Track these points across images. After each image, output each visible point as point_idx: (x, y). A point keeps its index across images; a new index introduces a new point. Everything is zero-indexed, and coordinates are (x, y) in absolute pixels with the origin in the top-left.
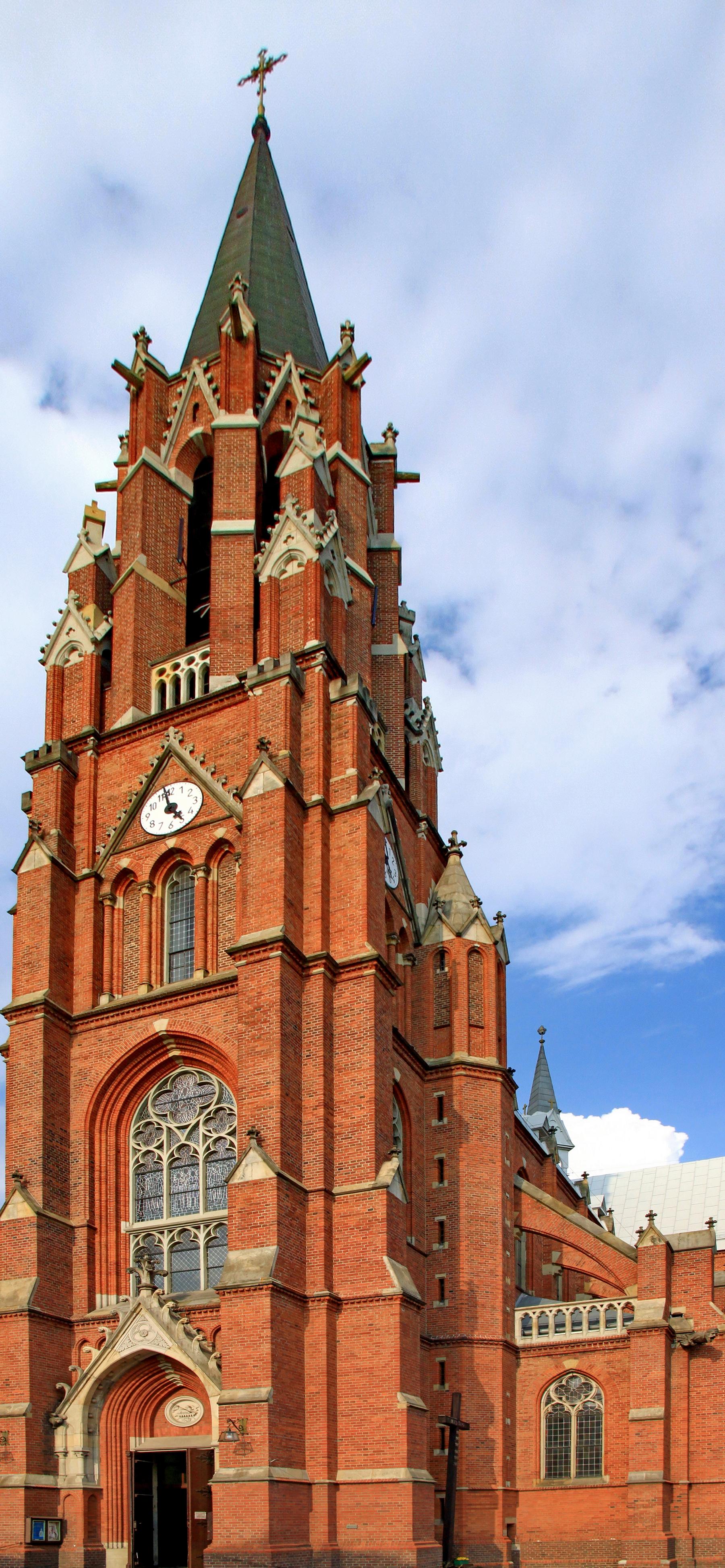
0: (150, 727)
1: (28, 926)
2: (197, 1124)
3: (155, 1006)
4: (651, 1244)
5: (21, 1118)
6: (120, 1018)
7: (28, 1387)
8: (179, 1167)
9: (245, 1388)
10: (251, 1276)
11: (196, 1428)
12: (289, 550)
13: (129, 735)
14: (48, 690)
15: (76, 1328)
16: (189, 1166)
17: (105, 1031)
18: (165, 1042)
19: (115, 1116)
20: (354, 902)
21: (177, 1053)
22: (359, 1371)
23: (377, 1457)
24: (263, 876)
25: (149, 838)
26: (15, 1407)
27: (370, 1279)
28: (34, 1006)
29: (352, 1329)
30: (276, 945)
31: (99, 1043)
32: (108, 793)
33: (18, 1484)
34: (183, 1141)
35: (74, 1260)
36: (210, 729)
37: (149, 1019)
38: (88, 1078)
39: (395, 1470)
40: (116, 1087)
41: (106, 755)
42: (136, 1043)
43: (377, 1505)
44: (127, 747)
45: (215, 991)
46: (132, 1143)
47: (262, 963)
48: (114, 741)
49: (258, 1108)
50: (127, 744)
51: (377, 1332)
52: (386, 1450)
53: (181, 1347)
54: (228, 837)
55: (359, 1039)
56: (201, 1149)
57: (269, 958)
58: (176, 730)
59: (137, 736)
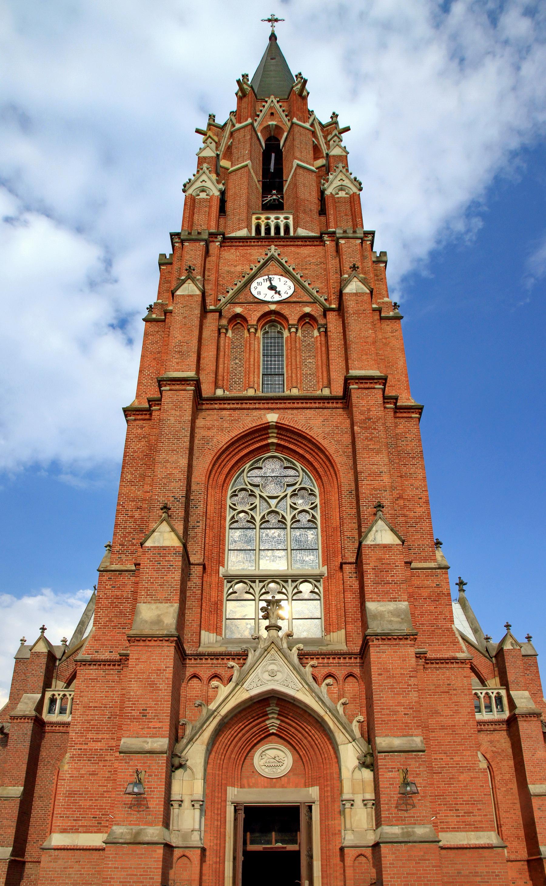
0: (258, 242)
1: (181, 328)
3: (268, 403)
4: (511, 647)
5: (167, 461)
6: (239, 406)
9: (398, 736)
10: (396, 626)
11: (285, 780)
12: (342, 185)
13: (243, 242)
14: (185, 204)
15: (188, 661)
17: (225, 413)
18: (270, 431)
19: (223, 477)
20: (400, 371)
21: (275, 441)
22: (443, 728)
23: (471, 819)
24: (361, 338)
25: (256, 300)
26: (153, 742)
27: (444, 644)
28: (188, 380)
29: (433, 688)
30: (380, 381)
32: (227, 268)
33: (156, 839)
34: (273, 508)
36: (298, 254)
37: (262, 412)
38: (211, 444)
39: (486, 833)
40: (227, 456)
41: (226, 248)
43: (476, 874)
44: (242, 248)
45: (315, 403)
47: (369, 390)
48: (232, 242)
50: (241, 246)
51: (455, 692)
52: (475, 811)
53: (312, 690)
54: (313, 313)
55: (413, 458)
56: (289, 518)
57: (374, 388)
58: (276, 248)
59: (248, 244)
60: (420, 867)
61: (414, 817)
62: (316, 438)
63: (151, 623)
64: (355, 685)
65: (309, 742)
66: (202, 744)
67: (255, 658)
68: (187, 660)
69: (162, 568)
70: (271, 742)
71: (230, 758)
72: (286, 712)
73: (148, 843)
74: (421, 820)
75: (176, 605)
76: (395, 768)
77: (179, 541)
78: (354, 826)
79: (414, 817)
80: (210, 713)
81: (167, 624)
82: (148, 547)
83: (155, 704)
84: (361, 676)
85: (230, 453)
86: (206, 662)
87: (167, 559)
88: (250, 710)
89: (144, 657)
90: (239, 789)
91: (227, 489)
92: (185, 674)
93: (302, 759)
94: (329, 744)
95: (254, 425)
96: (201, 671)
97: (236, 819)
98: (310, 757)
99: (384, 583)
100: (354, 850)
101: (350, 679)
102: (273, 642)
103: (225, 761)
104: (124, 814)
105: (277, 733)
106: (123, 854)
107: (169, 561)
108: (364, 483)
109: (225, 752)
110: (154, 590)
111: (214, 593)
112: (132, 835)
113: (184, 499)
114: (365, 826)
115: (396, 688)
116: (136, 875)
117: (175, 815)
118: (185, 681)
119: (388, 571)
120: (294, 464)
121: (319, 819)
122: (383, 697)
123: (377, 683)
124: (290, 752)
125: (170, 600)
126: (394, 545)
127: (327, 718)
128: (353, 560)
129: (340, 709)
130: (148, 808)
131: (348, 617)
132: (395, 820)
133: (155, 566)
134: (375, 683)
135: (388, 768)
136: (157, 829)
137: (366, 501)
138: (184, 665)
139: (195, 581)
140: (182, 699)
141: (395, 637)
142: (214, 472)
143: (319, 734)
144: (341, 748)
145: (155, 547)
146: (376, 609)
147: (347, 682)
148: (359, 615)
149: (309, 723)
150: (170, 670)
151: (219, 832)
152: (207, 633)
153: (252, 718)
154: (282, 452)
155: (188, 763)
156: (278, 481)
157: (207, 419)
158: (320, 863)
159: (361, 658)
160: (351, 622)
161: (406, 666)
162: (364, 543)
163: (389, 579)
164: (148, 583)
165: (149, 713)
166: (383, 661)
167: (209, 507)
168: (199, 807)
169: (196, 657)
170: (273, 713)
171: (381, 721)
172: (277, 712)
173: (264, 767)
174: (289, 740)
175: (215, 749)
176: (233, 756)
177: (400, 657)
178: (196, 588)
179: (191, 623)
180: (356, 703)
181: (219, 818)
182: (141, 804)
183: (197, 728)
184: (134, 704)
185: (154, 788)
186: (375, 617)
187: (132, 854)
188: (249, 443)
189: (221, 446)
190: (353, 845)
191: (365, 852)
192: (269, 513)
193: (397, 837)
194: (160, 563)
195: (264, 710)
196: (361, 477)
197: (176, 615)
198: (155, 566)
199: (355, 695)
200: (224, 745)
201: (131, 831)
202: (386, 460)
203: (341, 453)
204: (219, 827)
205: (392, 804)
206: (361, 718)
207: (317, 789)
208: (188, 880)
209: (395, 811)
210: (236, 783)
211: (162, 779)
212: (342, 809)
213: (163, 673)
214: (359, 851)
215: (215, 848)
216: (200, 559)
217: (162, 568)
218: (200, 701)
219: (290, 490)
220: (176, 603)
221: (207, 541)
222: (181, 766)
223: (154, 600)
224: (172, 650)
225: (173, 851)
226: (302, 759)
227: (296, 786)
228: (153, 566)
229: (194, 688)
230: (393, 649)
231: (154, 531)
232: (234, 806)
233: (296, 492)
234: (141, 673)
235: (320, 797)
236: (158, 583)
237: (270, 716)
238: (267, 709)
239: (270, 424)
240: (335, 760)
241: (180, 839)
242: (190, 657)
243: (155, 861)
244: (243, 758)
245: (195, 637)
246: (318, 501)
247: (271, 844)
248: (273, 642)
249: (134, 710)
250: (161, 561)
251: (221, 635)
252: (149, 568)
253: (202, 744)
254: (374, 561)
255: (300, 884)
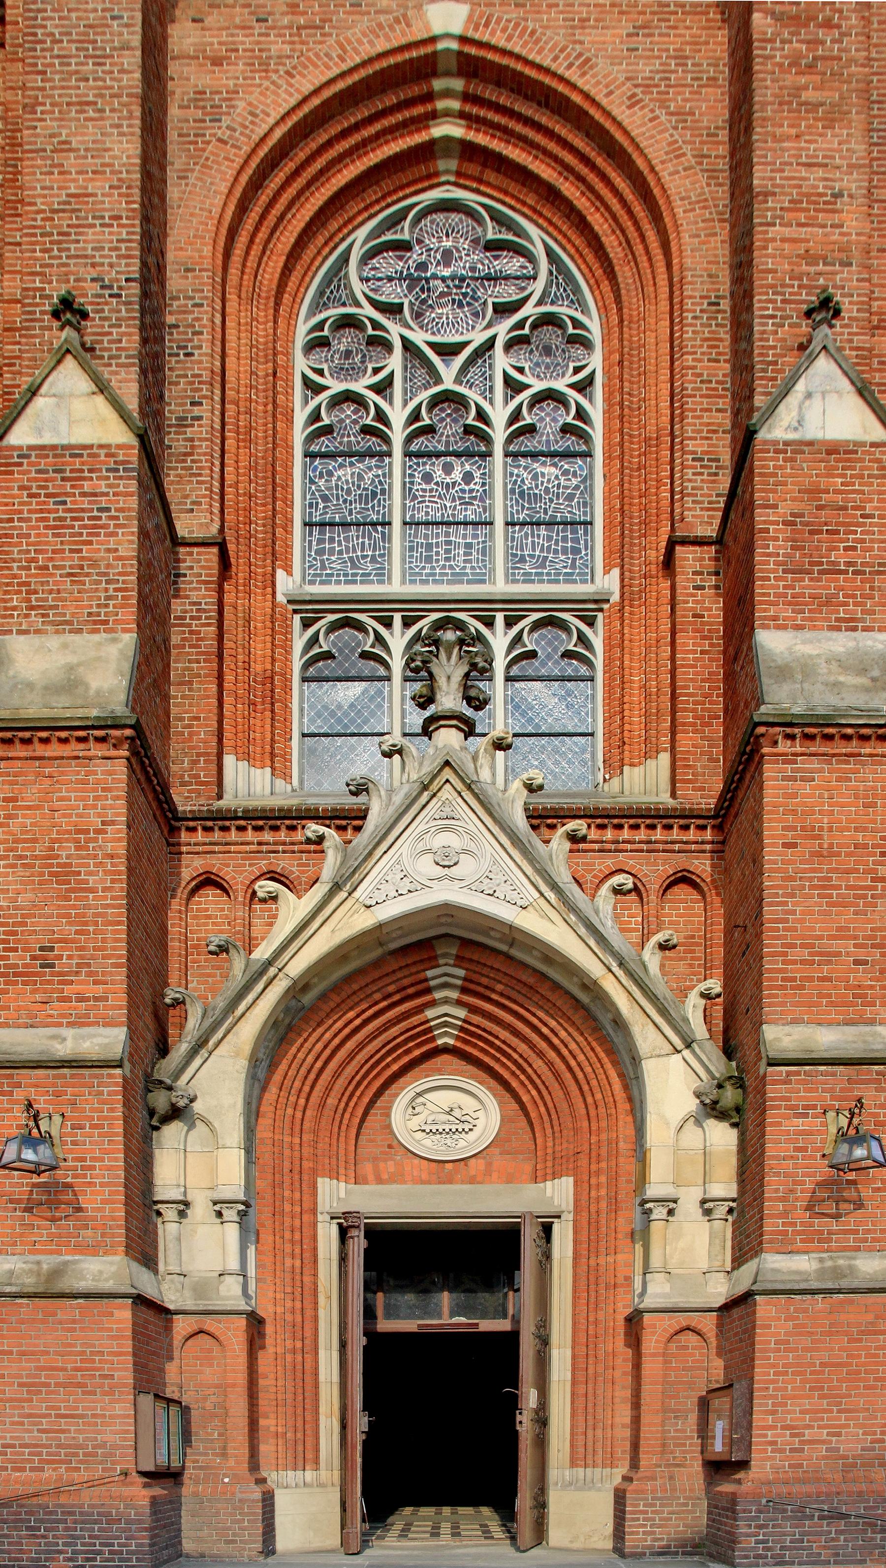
2: (490, 344)
7: (121, 975)
8: (429, 455)
9: (830, 1023)
15: (184, 836)
16: (458, 455)
18: (438, 84)
21: (454, 130)
31: (258, 28)
33: (108, 1285)
34: (448, 383)
35: (175, 639)
38: (226, 121)
42: (373, 52)
46: (301, 364)
49: (810, 258)
56: (499, 414)
60: (859, 1349)
61: (856, 1232)
62: (604, 102)
63: (46, 688)
64: (693, 908)
65: (550, 1064)
66: (237, 1055)
67: (391, 809)
68: (183, 834)
69: (73, 519)
70: (440, 1071)
71: (322, 1105)
72: (484, 981)
73: (87, 1296)
74: (874, 1240)
75: (128, 640)
76: (814, 1107)
77: (124, 427)
78: (673, 1262)
79: (856, 1232)
80: (255, 968)
81: (98, 692)
82: (20, 448)
83: (77, 932)
84: (713, 881)
85: (296, 173)
86: (240, 840)
87: (87, 486)
88: (377, 974)
89: (31, 794)
90: (351, 1186)
91: (293, 316)
92: (179, 874)
93: (527, 1115)
94: (608, 1066)
95: (381, 46)
96: (228, 866)
97: (343, 1259)
98: (550, 1105)
99: (821, 572)
100: (670, 1319)
101: (682, 892)
102: (447, 763)
103: (309, 1113)
104: (13, 1227)
105: (459, 1044)
106: (22, 1322)
107: (95, 495)
108: (772, 232)
109: (307, 1088)
110: (51, 592)
111: (260, 648)
112: (39, 1275)
113: (135, 289)
114: (704, 1264)
115: (839, 887)
116: (64, 1369)
117: (169, 1237)
118: (182, 893)
119: (837, 532)
120: (520, 232)
121: (570, 1253)
122: (794, 912)
123: (777, 870)
124: (495, 1095)
125: (106, 622)
126: (863, 444)
127: (609, 985)
128: (711, 531)
129: (652, 959)
130: (79, 1209)
131: (685, 710)
132: (802, 1241)
133: (49, 511)
134: (772, 870)
135: (797, 1107)
136: (111, 1263)
137: (774, 302)
138: (174, 850)
139: (194, 596)
140: (174, 945)
141: (849, 731)
142: (242, 240)
143: (580, 1039)
144: (649, 1067)
145: (43, 447)
146: (789, 649)
147: (670, 901)
148: (718, 703)
149: (554, 1011)
150: (119, 831)
151: (298, 1283)
152: (243, 765)
153: (385, 998)
154: (480, 181)
155: (197, 1107)
156: (465, 295)
157: (209, 21)
158: (569, 1353)
159: (719, 828)
160: (694, 725)
161: (874, 821)
162: (762, 435)
163: (839, 557)
164: (29, 568)
165: (60, 957)
166: (804, 804)
167: (231, 362)
168: (237, 1219)
169: (210, 824)
170: (445, 986)
171: (783, 979)
172: (459, 982)
173: (420, 1135)
174: (492, 1063)
175: (277, 1077)
176: (331, 1101)
177: (856, 796)
178: (200, 618)
179: (190, 726)
180: (692, 959)
181: (297, 1251)
182: (60, 1202)
183: (217, 1012)
184: (14, 933)
185: (93, 1159)
186: (784, 672)
187: (43, 1322)
188: (366, 133)
189: (265, 128)
190: (669, 1306)
191: (700, 1322)
192: (436, 402)
193: (807, 1280)
194: (65, 503)
195: (421, 976)
196: (764, 211)
197: (127, 667)
198: (49, 511)
199: (693, 937)
200: (303, 1070)
201: (35, 1267)
202: (860, 148)
203: (690, 159)
204: (298, 1271)
205: (797, 1199)
206: (715, 985)
207: (567, 1184)
208: (217, 1386)
209: (801, 1216)
210: (342, 1171)
211: (116, 1134)
212: (638, 1226)
213: (96, 840)
214: (682, 1320)
215: (289, 1317)
216: (207, 525)
217: (73, 519)
218: (224, 936)
219: (503, 329)
220: (125, 631)
221: (230, 479)
222: (175, 1113)
223: (52, 623)
224: (120, 770)
225: (171, 1321)
226: (527, 1115)
227: (510, 1180)
228: (41, 511)
229: (209, 917)
230: (838, 770)
231: (34, 392)
232: (340, 1225)
233: (526, 331)
234: (25, 841)
235: (576, 1201)
236: (63, 567)
237: (438, 995)
238: (430, 973)
239: (440, 46)
240: (624, 1107)
241: (187, 1293)
242: (191, 824)
243: (112, 1338)
244: (360, 1112)
245: (203, 769)
246: (596, 362)
247: (440, 1318)
248: (447, 763)
249: (15, 950)
250: (66, 494)
251: (287, 776)
252: (29, 520)
253: (237, 1055)
254: (793, 499)
255: (516, 1396)
